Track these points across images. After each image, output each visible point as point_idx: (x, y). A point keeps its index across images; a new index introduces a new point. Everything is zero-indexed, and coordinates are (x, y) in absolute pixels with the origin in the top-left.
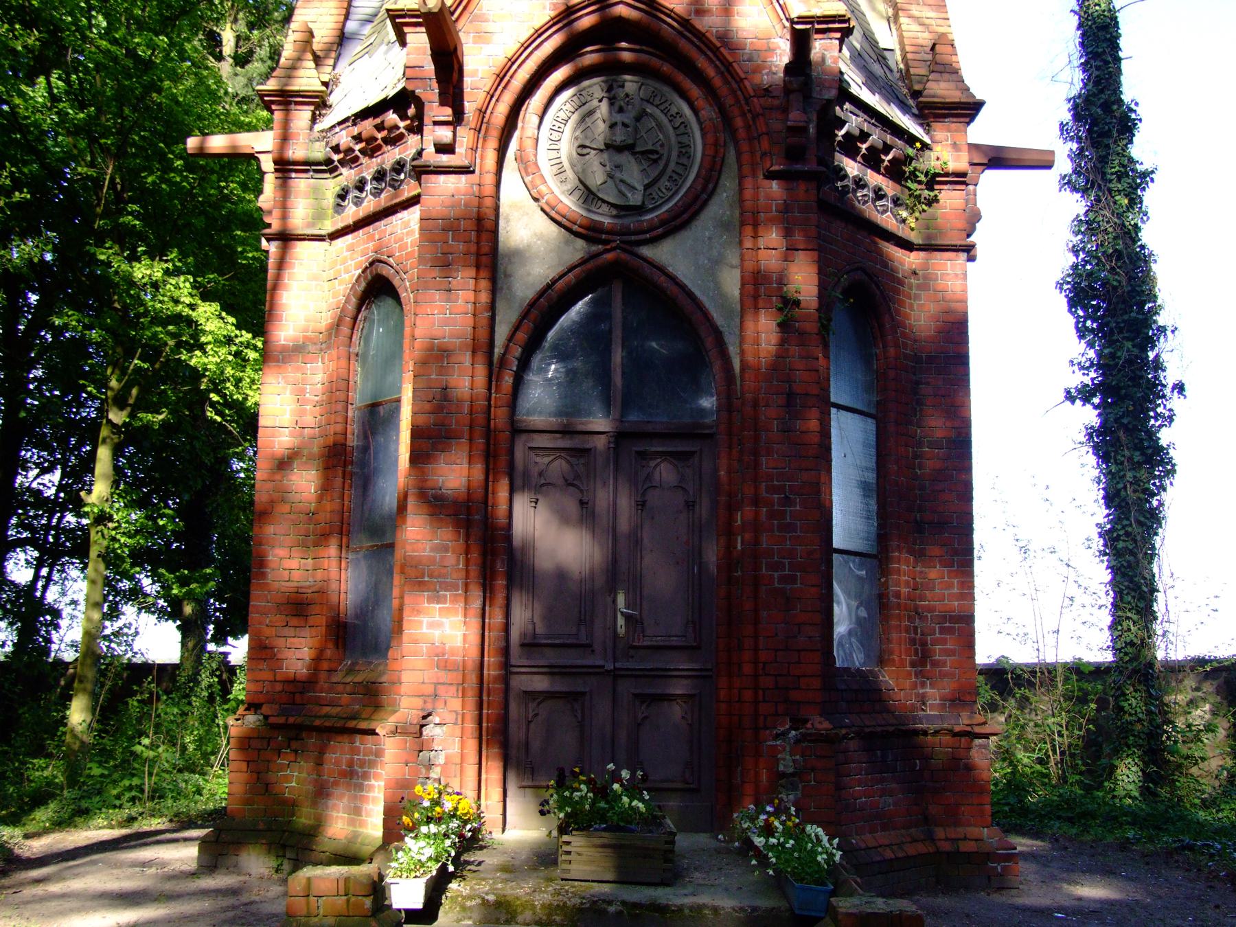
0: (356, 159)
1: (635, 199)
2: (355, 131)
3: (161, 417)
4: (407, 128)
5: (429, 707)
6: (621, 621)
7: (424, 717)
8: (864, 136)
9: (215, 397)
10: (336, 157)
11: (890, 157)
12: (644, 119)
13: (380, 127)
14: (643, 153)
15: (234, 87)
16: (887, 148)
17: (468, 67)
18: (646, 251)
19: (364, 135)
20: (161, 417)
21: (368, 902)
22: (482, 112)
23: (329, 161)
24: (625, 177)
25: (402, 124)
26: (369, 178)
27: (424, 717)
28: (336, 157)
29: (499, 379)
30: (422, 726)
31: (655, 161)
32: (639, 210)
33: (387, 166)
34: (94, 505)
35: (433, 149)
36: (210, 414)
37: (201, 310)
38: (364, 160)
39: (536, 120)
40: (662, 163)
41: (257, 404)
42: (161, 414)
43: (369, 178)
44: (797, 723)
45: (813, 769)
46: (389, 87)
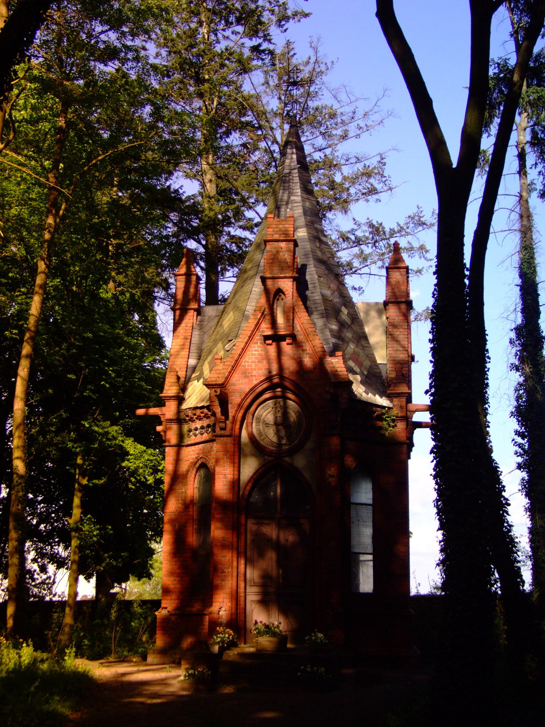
3: (102, 481)
4: (196, 418)
5: (221, 605)
7: (220, 608)
9: (133, 480)
10: (187, 418)
13: (202, 413)
20: (102, 481)
22: (234, 417)
25: (209, 413)
26: (199, 428)
27: (220, 608)
30: (219, 611)
33: (205, 425)
35: (219, 429)
36: (130, 486)
37: (127, 442)
41: (363, 303)
42: (102, 480)
43: (199, 428)
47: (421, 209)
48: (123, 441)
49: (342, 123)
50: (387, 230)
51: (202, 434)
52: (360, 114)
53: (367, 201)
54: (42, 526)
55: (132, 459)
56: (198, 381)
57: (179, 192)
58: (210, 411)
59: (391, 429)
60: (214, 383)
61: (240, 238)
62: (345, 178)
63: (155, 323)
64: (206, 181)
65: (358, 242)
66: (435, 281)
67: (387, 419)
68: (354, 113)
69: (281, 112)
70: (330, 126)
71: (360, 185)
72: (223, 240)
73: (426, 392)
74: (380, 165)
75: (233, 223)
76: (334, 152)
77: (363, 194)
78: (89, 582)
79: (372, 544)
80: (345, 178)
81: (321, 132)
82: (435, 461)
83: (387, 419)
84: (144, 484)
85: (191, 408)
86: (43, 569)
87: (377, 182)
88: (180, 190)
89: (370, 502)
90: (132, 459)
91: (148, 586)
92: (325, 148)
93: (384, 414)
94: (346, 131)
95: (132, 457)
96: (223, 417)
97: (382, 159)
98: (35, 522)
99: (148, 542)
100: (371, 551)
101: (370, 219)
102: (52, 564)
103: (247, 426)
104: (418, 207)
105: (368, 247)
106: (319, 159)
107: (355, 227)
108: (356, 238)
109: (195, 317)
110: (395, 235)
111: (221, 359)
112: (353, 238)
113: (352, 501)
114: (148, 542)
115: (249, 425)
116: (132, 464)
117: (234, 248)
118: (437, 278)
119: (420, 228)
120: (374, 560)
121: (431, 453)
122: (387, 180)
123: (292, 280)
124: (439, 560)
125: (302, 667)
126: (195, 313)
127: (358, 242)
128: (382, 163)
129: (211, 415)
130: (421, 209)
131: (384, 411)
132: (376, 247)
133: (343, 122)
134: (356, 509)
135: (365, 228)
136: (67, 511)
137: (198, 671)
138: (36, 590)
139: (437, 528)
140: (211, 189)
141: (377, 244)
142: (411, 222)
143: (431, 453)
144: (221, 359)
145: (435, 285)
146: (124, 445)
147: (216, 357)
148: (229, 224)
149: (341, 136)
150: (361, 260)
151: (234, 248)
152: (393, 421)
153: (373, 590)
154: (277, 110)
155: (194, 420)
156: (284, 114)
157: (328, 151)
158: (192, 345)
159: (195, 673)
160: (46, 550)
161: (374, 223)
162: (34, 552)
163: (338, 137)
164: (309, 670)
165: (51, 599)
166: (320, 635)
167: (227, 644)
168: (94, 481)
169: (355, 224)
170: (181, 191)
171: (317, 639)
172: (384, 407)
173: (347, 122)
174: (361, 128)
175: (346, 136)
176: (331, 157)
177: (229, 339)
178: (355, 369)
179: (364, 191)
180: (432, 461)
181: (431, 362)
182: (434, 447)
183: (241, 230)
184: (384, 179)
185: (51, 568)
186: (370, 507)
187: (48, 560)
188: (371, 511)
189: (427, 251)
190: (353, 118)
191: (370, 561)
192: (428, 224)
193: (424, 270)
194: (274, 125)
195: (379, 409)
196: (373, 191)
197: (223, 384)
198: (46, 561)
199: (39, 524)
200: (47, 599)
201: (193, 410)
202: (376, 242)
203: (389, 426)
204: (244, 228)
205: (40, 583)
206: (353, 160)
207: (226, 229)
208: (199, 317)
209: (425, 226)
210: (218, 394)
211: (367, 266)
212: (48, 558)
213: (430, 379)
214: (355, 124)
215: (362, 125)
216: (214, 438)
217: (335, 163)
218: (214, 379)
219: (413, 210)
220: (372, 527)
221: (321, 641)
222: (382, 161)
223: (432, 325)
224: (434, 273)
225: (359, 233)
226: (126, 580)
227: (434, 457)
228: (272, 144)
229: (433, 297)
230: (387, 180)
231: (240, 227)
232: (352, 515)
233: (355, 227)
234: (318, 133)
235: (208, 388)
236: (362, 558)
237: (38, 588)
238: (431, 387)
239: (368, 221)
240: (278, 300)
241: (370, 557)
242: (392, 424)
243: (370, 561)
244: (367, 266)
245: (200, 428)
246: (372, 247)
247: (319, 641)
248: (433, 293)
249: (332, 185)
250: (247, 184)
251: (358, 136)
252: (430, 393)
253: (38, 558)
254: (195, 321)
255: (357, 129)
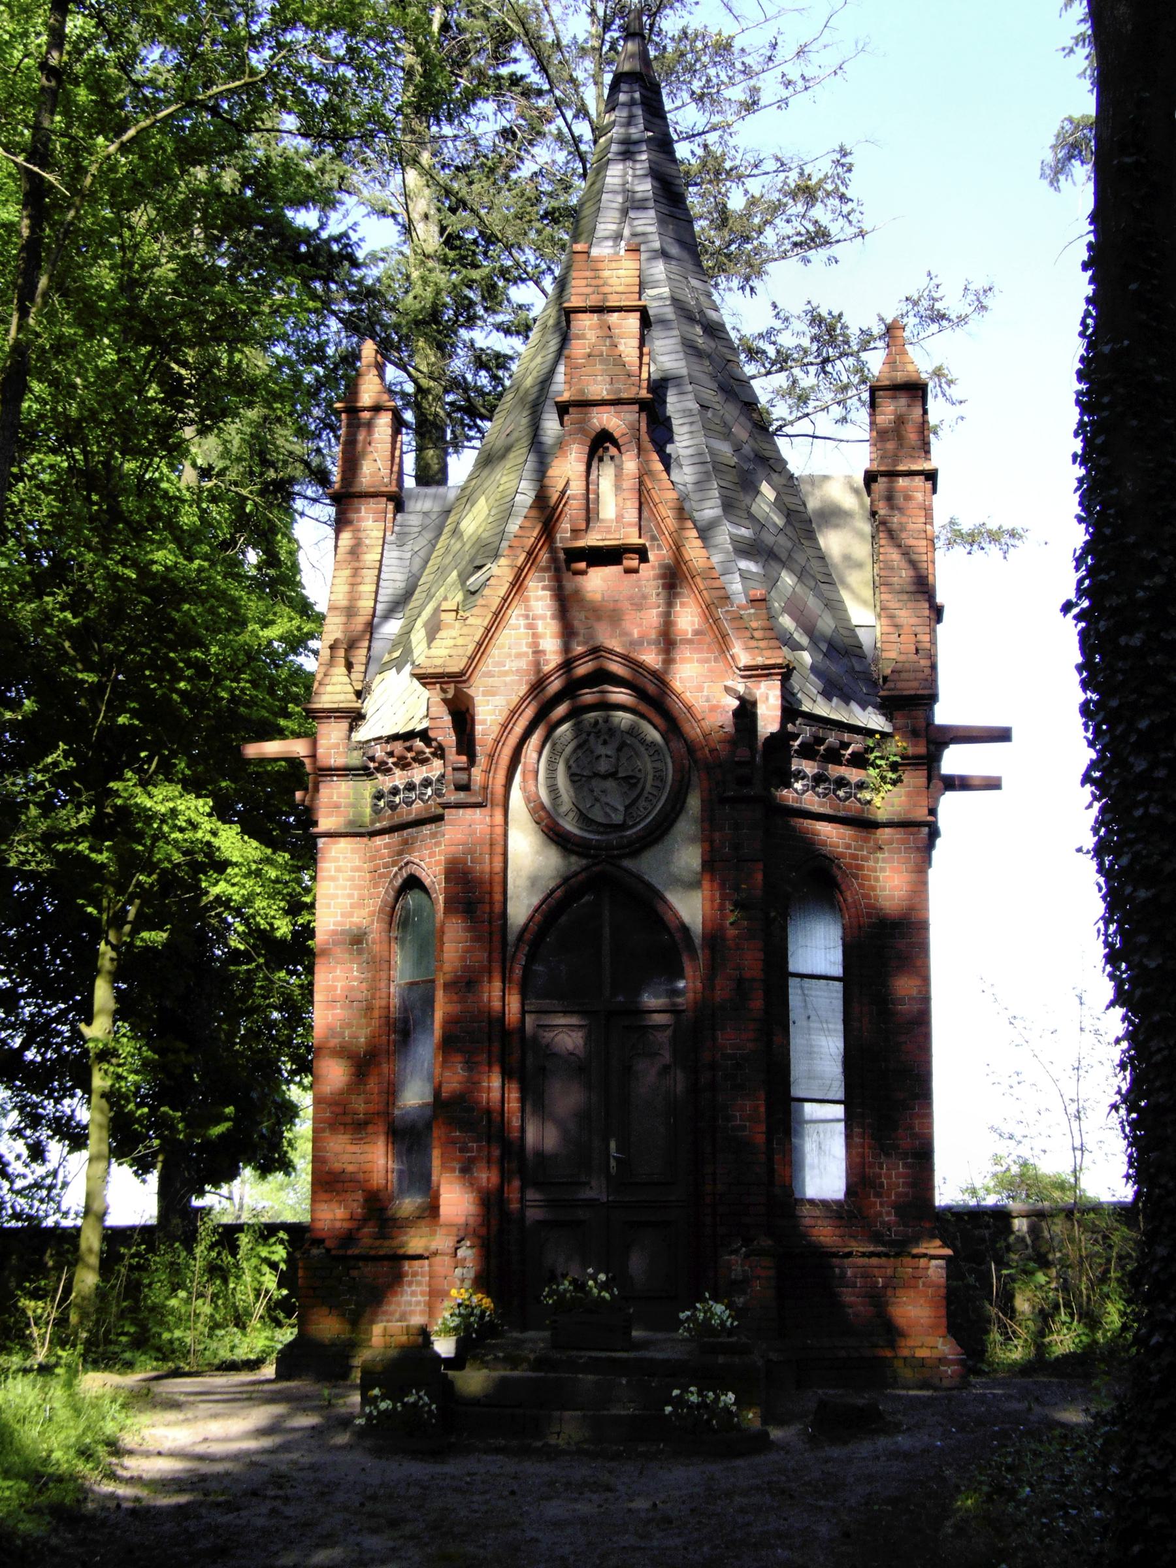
0: (390, 770)
1: (618, 818)
2: (389, 748)
6: (613, 1163)
8: (820, 741)
10: (372, 765)
11: (850, 751)
12: (625, 749)
13: (409, 749)
14: (624, 778)
15: (205, 456)
16: (845, 746)
17: (479, 717)
18: (627, 863)
19: (396, 753)
21: (420, 1339)
23: (366, 768)
24: (608, 800)
25: (427, 750)
28: (372, 765)
29: (511, 971)
31: (635, 785)
32: (622, 827)
33: (417, 780)
34: (95, 1040)
38: (397, 772)
39: (535, 755)
40: (640, 786)
44: (747, 1241)
45: (758, 1278)
46: (416, 720)
47: (936, 281)
48: (214, 834)
49: (744, 72)
50: (853, 332)
51: (409, 804)
52: (786, 51)
53: (806, 261)
54: (30, 1055)
55: (236, 875)
56: (398, 672)
57: (349, 238)
58: (428, 745)
59: (889, 787)
60: (440, 670)
61: (498, 355)
62: (753, 202)
63: (295, 568)
64: (415, 216)
65: (783, 361)
66: (1089, 290)
67: (879, 762)
68: (774, 46)
69: (597, 44)
70: (715, 81)
71: (788, 221)
72: (459, 364)
73: (1067, 607)
74: (840, 169)
75: (481, 318)
76: (726, 137)
77: (795, 244)
78: (144, 1181)
79: (841, 1077)
80: (753, 202)
81: (693, 93)
82: (1097, 805)
83: (879, 762)
84: (262, 938)
85: (380, 738)
86: (37, 1153)
87: (830, 216)
88: (351, 232)
89: (838, 971)
90: (236, 875)
91: (292, 1194)
92: (704, 133)
93: (872, 750)
94: (755, 90)
95: (236, 870)
96: (464, 758)
97: (845, 155)
98: (17, 1042)
99: (284, 1087)
100: (840, 1095)
101: (814, 304)
102: (59, 1141)
103: (524, 780)
104: (929, 274)
105: (807, 373)
106: (689, 156)
107: (778, 324)
108: (778, 352)
109: (390, 516)
110: (872, 345)
111: (457, 611)
112: (771, 352)
113: (792, 968)
114: (284, 1087)
115: (530, 776)
116: (236, 889)
117: (484, 379)
118: (1092, 281)
119: (934, 327)
120: (850, 1120)
121: (1083, 783)
122: (853, 210)
123: (636, 408)
124: (1119, 1092)
125: (676, 1392)
126: (391, 506)
127: (783, 361)
128: (843, 165)
129: (434, 754)
130: (936, 281)
131: (871, 743)
132: (825, 373)
133: (747, 71)
134: (802, 988)
135: (801, 326)
136: (87, 1013)
137: (404, 1405)
138: (22, 1201)
139: (1107, 1002)
140: (429, 237)
141: (829, 368)
142: (911, 314)
143: (1083, 783)
144: (457, 611)
145: (1089, 301)
146: (216, 842)
147: (445, 606)
148: (471, 322)
149: (741, 104)
150: (790, 401)
151: (484, 379)
152: (894, 767)
153: (850, 1190)
154: (586, 41)
155: (390, 770)
156: (605, 49)
157: (712, 138)
158: (382, 583)
159: (395, 1408)
160: (44, 1108)
161: (825, 314)
162: (16, 1112)
163: (735, 107)
164: (694, 1398)
165: (57, 1223)
166: (719, 1308)
167: (476, 1331)
168: (145, 935)
169: (777, 316)
170: (354, 237)
171: (710, 1319)
172: (870, 733)
173: (756, 68)
174: (790, 82)
175: (754, 103)
176: (718, 150)
177: (477, 563)
178: (796, 636)
179: (797, 239)
180: (1090, 806)
181: (1080, 520)
182: (1093, 765)
183: (501, 335)
184: (846, 209)
185: (55, 1149)
186: (839, 986)
187: (50, 1133)
188: (841, 995)
189: (950, 383)
190: (770, 59)
191: (838, 1120)
192: (953, 317)
193: (945, 426)
194: (580, 75)
195: (858, 737)
196: (819, 237)
197: (462, 673)
198: (44, 1133)
199: (25, 1046)
200: (49, 1222)
201: (387, 742)
202: (827, 360)
203: (883, 778)
204: (506, 330)
205: (30, 1187)
206: (770, 165)
207: (464, 334)
208: (399, 516)
209: (945, 323)
210: (450, 696)
211: (807, 415)
212: (49, 1127)
213: (1077, 569)
214: (777, 72)
215: (794, 74)
216: (440, 811)
217: (728, 165)
218: (438, 662)
219: (915, 285)
220: (841, 1035)
221: (723, 1323)
222: (843, 161)
223: (1081, 414)
224: (1085, 266)
225: (787, 340)
226: (231, 1175)
227: (1093, 793)
228: (576, 117)
229: (1082, 335)
230: (853, 210)
231: (499, 327)
232: (791, 1003)
233: (778, 324)
234: (686, 96)
235: (424, 685)
236: (811, 1110)
237: (26, 1196)
238: (1081, 592)
239: (809, 307)
240: (601, 460)
241: (839, 1111)
242: (890, 775)
243: (838, 1120)
244: (807, 415)
245: (405, 789)
246: (817, 375)
247: (715, 1322)
248: (1083, 324)
249: (723, 217)
250: (516, 217)
251: (783, 103)
252: (1076, 611)
253: (25, 1128)
254: (389, 525)
255: (782, 87)
